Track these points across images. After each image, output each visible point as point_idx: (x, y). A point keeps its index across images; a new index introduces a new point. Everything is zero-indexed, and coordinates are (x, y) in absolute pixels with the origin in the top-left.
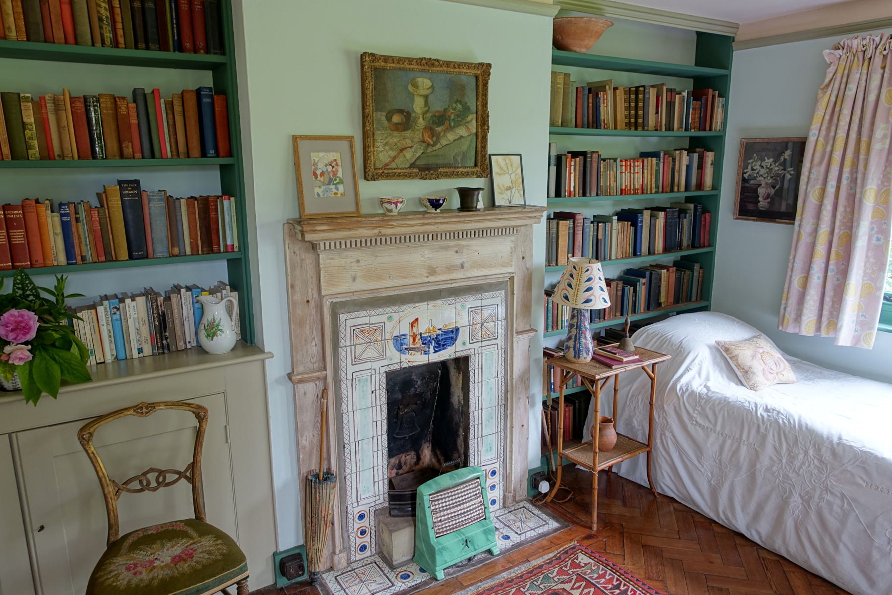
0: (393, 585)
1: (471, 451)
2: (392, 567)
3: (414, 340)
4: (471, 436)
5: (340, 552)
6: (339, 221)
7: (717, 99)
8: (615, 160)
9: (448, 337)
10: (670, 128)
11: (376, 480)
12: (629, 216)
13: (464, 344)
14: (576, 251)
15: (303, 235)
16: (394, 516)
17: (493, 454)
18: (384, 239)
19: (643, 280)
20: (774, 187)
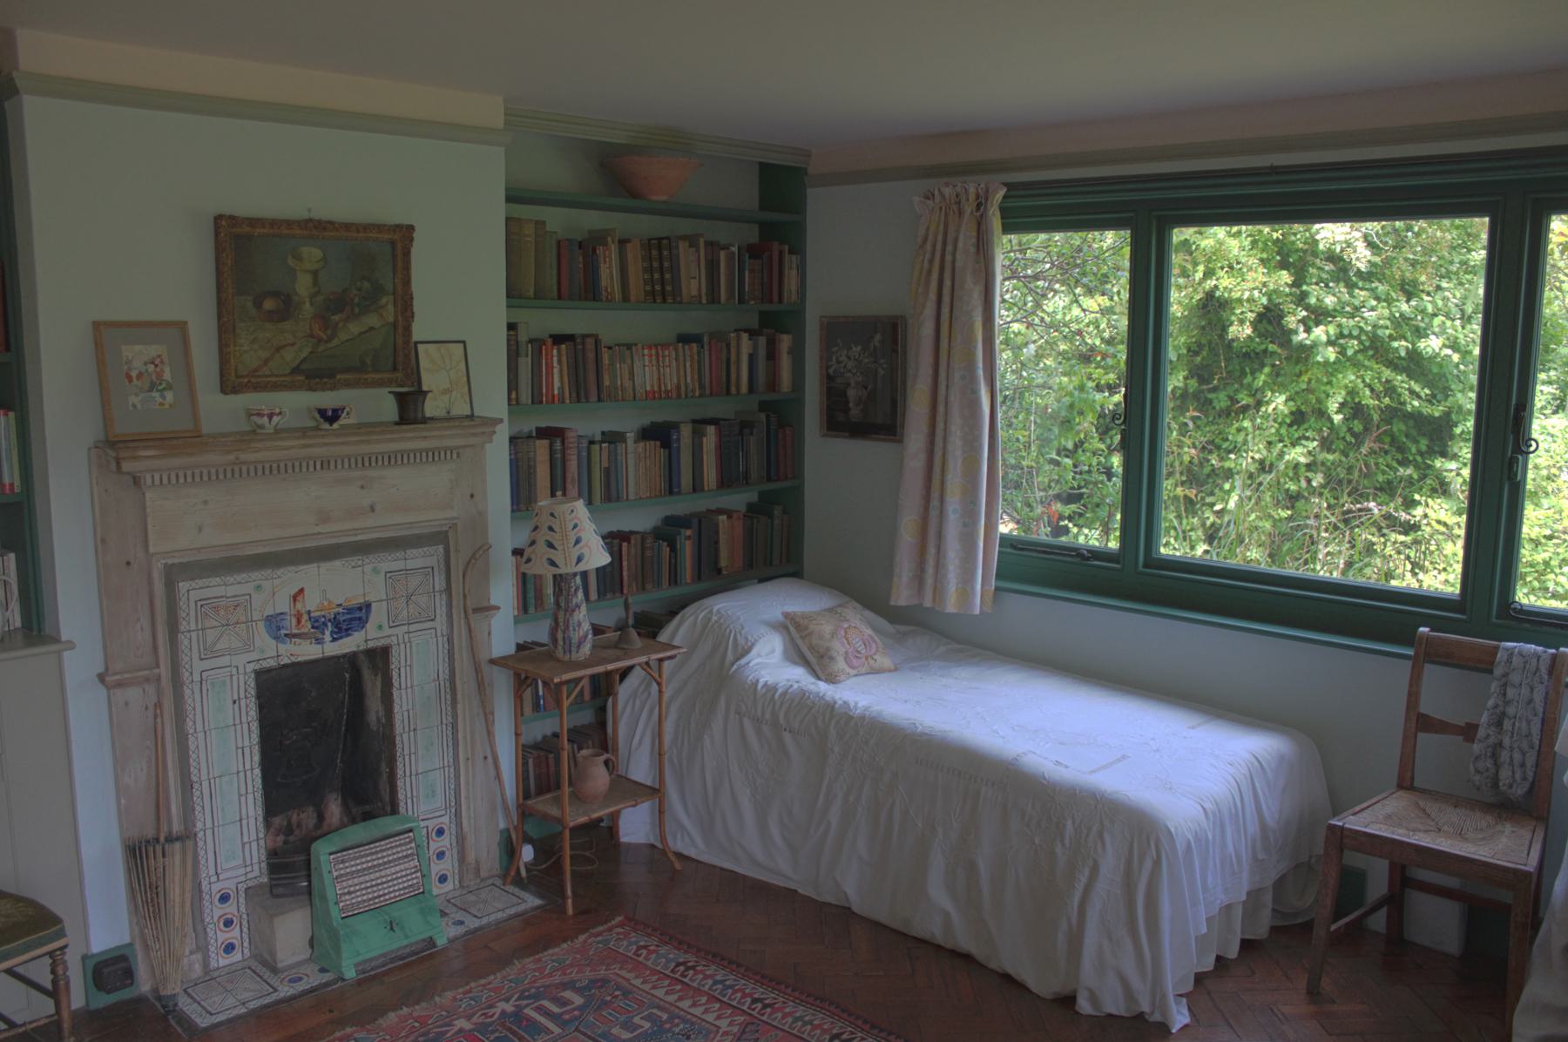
0: (276, 990)
1: (401, 796)
2: (275, 971)
3: (299, 622)
4: (400, 772)
5: (192, 953)
6: (174, 442)
7: (787, 256)
8: (629, 347)
9: (352, 618)
10: (713, 298)
11: (246, 839)
12: (658, 434)
13: (380, 627)
14: (569, 486)
15: (118, 463)
16: (278, 896)
17: (439, 802)
18: (244, 468)
19: (688, 532)
20: (866, 388)
